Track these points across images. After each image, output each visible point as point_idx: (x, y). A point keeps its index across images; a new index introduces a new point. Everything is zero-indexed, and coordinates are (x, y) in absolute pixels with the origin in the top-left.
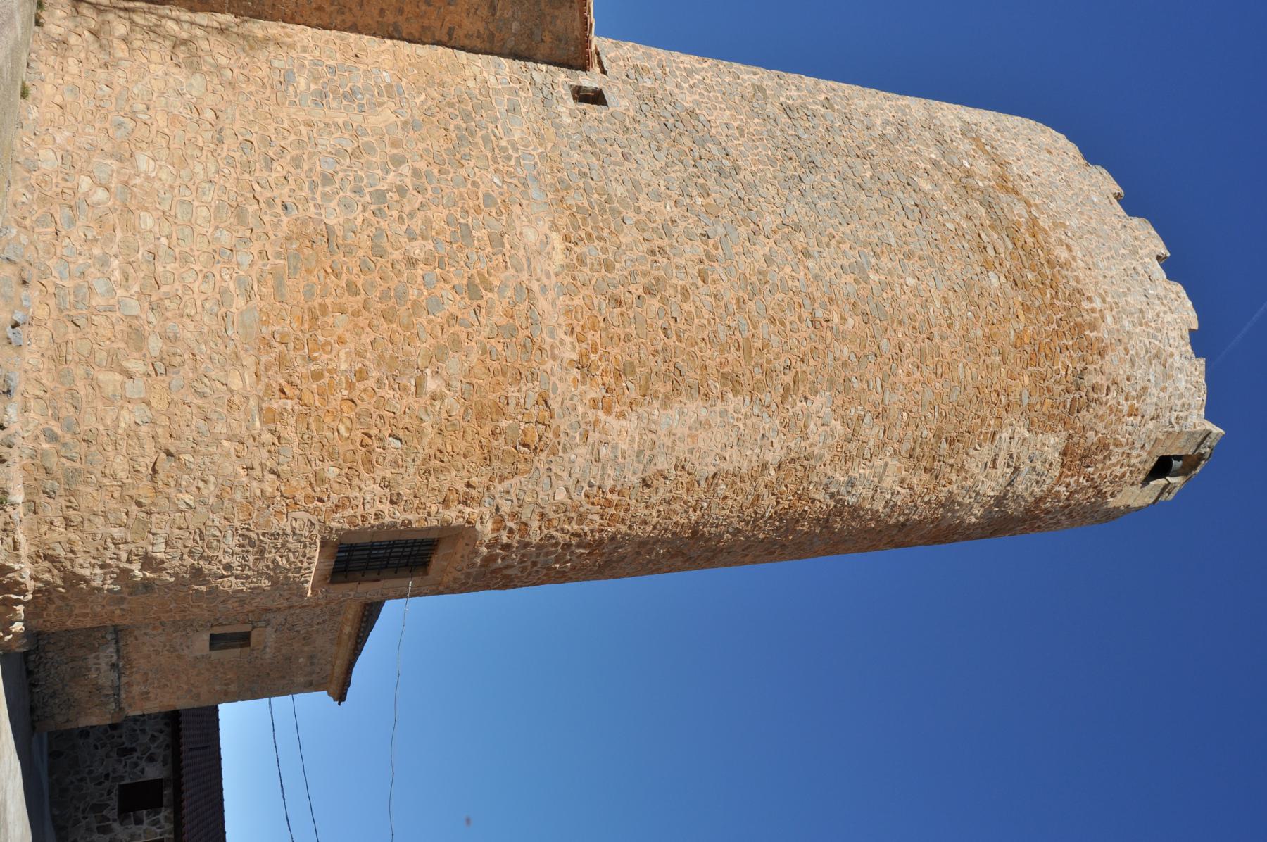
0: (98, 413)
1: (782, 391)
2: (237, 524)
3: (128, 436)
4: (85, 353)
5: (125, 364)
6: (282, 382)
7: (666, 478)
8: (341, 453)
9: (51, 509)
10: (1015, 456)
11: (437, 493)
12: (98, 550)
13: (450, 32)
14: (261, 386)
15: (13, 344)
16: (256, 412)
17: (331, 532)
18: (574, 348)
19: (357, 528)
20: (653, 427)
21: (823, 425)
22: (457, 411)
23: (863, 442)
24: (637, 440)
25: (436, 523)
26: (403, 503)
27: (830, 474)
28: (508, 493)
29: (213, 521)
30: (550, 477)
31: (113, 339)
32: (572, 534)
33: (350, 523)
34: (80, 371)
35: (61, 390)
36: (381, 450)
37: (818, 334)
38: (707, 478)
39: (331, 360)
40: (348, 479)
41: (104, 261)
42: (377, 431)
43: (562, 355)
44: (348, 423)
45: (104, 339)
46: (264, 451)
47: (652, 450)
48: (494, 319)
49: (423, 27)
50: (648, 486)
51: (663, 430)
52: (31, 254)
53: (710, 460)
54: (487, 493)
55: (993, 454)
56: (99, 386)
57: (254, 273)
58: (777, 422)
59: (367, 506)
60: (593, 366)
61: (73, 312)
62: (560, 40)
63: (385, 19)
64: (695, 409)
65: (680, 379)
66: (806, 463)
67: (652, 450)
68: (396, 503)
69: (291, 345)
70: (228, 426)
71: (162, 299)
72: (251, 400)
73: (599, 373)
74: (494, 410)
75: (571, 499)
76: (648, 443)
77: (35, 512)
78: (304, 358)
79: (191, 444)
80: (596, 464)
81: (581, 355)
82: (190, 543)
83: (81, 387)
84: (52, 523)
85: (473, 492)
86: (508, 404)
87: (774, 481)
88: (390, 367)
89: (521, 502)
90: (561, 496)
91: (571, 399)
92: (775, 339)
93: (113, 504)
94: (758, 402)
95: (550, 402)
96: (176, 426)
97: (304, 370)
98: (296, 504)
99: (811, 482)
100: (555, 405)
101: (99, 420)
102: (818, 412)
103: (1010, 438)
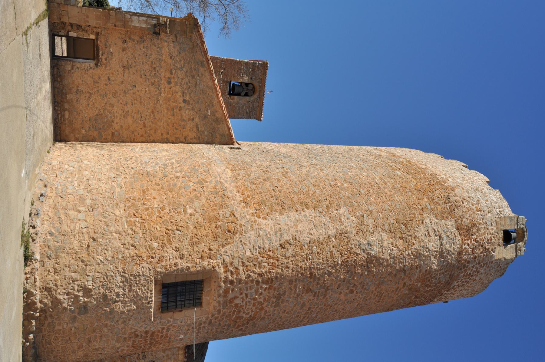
0: (68, 225)
1: (326, 207)
2: (120, 270)
3: (79, 233)
4: (65, 206)
5: (78, 208)
6: (134, 212)
7: (290, 244)
8: (158, 237)
9: (50, 264)
10: (436, 230)
11: (198, 253)
12: (66, 285)
13: (185, 138)
14: (127, 213)
15: (41, 201)
16: (125, 222)
17: (158, 274)
18: (241, 197)
19: (168, 272)
20: (278, 222)
21: (347, 219)
22: (201, 219)
23: (367, 226)
24: (273, 228)
25: (200, 268)
26: (185, 258)
27: (358, 239)
28: (226, 252)
29: (111, 268)
30: (242, 244)
31: (74, 201)
32: (258, 274)
33: (165, 269)
34: (63, 211)
35: (56, 218)
36: (173, 235)
37: (334, 189)
38: (307, 243)
39: (151, 204)
40: (162, 247)
41: (72, 182)
42: (171, 228)
43: (237, 199)
44: (160, 225)
45: (71, 201)
46: (129, 237)
47: (280, 231)
48: (209, 189)
49: (176, 138)
50: (284, 248)
51: (282, 223)
52: (48, 180)
53: (305, 235)
54: (218, 253)
55: (426, 230)
56: (69, 216)
57: (123, 182)
58: (328, 218)
59: (171, 260)
60: (249, 202)
61: (61, 194)
62: (222, 136)
63: (163, 137)
64: (293, 215)
65: (284, 205)
66: (346, 235)
67: (280, 231)
68: (182, 259)
69: (137, 200)
70: (115, 228)
71: (91, 190)
72: (123, 218)
73: (252, 204)
74: (214, 218)
75: (253, 255)
76: (278, 229)
77: (43, 266)
78: (141, 204)
79: (102, 235)
80: (259, 238)
81: (244, 199)
82: (102, 280)
83: (63, 217)
84: (49, 271)
85: (212, 252)
86: (219, 216)
87: (336, 244)
88: (173, 205)
89: (232, 257)
90: (248, 253)
91: (243, 213)
92: (317, 191)
93: (73, 261)
94: (318, 211)
95: (235, 215)
96: (96, 228)
97: (142, 208)
98: (143, 260)
99: (352, 244)
100: (238, 216)
101: (69, 227)
102: (343, 214)
103: (430, 223)
